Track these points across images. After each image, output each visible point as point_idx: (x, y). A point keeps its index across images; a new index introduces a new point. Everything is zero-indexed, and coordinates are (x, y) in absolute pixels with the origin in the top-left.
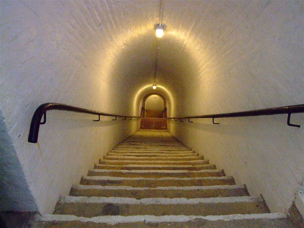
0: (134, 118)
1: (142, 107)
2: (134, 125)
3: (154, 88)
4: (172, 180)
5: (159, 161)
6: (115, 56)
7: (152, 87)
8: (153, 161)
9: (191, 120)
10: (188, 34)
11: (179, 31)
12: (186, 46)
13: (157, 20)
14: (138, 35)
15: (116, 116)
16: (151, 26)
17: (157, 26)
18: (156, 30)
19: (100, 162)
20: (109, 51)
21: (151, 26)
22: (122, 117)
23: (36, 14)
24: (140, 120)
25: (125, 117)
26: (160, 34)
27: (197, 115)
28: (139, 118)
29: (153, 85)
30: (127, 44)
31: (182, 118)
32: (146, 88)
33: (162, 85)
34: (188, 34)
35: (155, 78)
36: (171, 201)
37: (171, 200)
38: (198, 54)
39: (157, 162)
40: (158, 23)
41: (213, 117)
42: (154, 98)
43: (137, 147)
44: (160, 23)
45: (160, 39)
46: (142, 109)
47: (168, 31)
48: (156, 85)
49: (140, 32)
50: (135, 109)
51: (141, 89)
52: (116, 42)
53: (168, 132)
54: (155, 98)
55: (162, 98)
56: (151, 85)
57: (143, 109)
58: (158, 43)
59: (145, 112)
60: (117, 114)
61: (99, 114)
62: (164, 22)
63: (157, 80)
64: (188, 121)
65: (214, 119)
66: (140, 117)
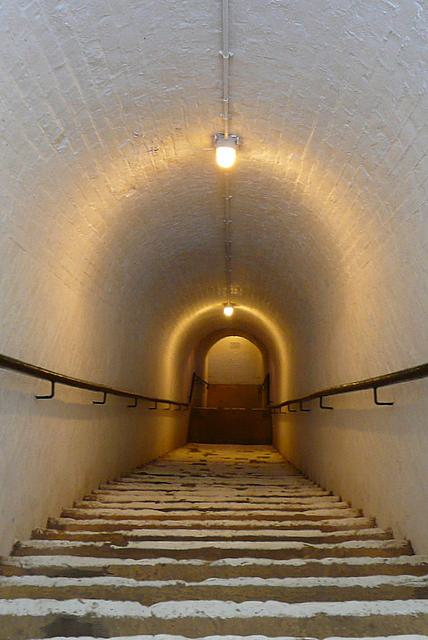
0: (167, 406)
1: (194, 374)
2: (166, 426)
3: (228, 312)
4: (254, 565)
5: (228, 523)
6: (103, 217)
7: (222, 311)
8: (206, 522)
9: (328, 400)
10: (302, 157)
11: (279, 152)
12: (302, 192)
13: (217, 123)
14: (170, 161)
15: (106, 390)
16: (201, 139)
17: (217, 139)
18: (215, 148)
19: (50, 525)
20: (85, 207)
21: (201, 139)
22: (126, 399)
23: (227, 65)
24: (188, 413)
25: (136, 397)
26: (226, 158)
27: (337, 384)
28: (183, 407)
29: (225, 305)
30: (137, 186)
31: (306, 399)
32: (204, 314)
33: (252, 306)
34: (302, 157)
35: (228, 284)
36: (238, 610)
37: (239, 606)
38: (333, 211)
39: (220, 522)
40: (219, 130)
41: (374, 384)
42: (231, 345)
43: (168, 488)
44: (226, 127)
45: (229, 171)
46: (193, 381)
47: (250, 150)
48: (233, 305)
49: (172, 154)
50: (168, 382)
51: (189, 316)
52: (106, 182)
53: (276, 449)
54: (235, 345)
55: (261, 350)
56: (219, 304)
57: (197, 379)
58: (227, 186)
59: (206, 390)
60: (106, 384)
61: (54, 378)
62: (237, 128)
63: (234, 290)
64: (319, 404)
65: (378, 389)
66: (187, 405)
